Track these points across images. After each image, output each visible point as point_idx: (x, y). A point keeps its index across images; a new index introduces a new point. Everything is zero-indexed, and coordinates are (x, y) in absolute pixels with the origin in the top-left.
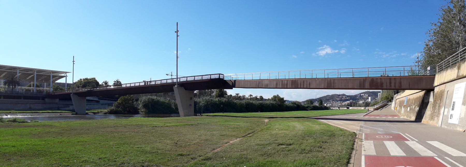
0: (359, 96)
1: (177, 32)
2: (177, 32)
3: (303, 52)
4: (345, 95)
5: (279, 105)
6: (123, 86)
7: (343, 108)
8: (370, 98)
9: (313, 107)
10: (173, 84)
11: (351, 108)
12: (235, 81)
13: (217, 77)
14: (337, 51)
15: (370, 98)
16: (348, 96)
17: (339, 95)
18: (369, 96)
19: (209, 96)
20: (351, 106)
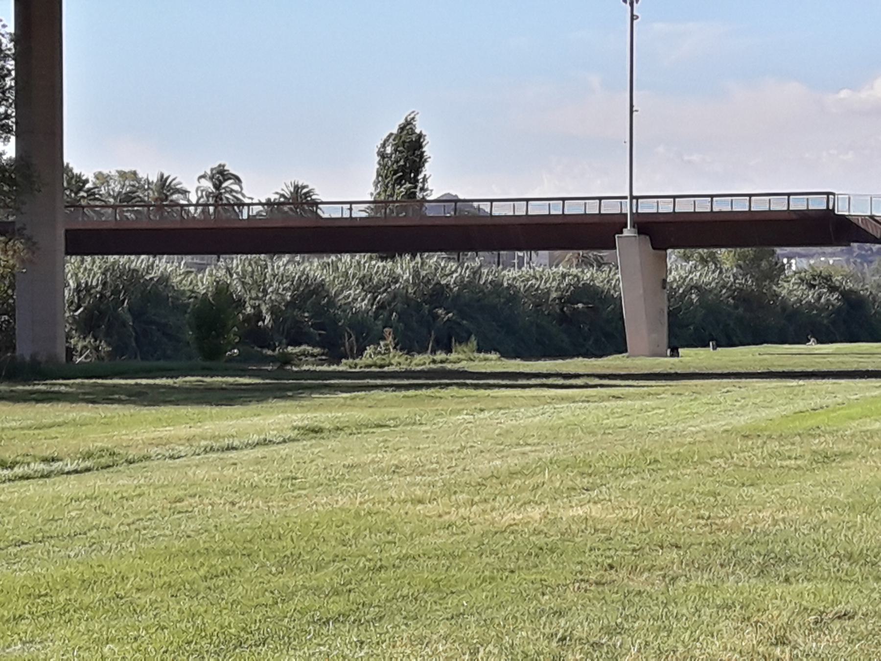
5: (743, 298)
6: (326, 212)
10: (616, 223)
13: (818, 204)
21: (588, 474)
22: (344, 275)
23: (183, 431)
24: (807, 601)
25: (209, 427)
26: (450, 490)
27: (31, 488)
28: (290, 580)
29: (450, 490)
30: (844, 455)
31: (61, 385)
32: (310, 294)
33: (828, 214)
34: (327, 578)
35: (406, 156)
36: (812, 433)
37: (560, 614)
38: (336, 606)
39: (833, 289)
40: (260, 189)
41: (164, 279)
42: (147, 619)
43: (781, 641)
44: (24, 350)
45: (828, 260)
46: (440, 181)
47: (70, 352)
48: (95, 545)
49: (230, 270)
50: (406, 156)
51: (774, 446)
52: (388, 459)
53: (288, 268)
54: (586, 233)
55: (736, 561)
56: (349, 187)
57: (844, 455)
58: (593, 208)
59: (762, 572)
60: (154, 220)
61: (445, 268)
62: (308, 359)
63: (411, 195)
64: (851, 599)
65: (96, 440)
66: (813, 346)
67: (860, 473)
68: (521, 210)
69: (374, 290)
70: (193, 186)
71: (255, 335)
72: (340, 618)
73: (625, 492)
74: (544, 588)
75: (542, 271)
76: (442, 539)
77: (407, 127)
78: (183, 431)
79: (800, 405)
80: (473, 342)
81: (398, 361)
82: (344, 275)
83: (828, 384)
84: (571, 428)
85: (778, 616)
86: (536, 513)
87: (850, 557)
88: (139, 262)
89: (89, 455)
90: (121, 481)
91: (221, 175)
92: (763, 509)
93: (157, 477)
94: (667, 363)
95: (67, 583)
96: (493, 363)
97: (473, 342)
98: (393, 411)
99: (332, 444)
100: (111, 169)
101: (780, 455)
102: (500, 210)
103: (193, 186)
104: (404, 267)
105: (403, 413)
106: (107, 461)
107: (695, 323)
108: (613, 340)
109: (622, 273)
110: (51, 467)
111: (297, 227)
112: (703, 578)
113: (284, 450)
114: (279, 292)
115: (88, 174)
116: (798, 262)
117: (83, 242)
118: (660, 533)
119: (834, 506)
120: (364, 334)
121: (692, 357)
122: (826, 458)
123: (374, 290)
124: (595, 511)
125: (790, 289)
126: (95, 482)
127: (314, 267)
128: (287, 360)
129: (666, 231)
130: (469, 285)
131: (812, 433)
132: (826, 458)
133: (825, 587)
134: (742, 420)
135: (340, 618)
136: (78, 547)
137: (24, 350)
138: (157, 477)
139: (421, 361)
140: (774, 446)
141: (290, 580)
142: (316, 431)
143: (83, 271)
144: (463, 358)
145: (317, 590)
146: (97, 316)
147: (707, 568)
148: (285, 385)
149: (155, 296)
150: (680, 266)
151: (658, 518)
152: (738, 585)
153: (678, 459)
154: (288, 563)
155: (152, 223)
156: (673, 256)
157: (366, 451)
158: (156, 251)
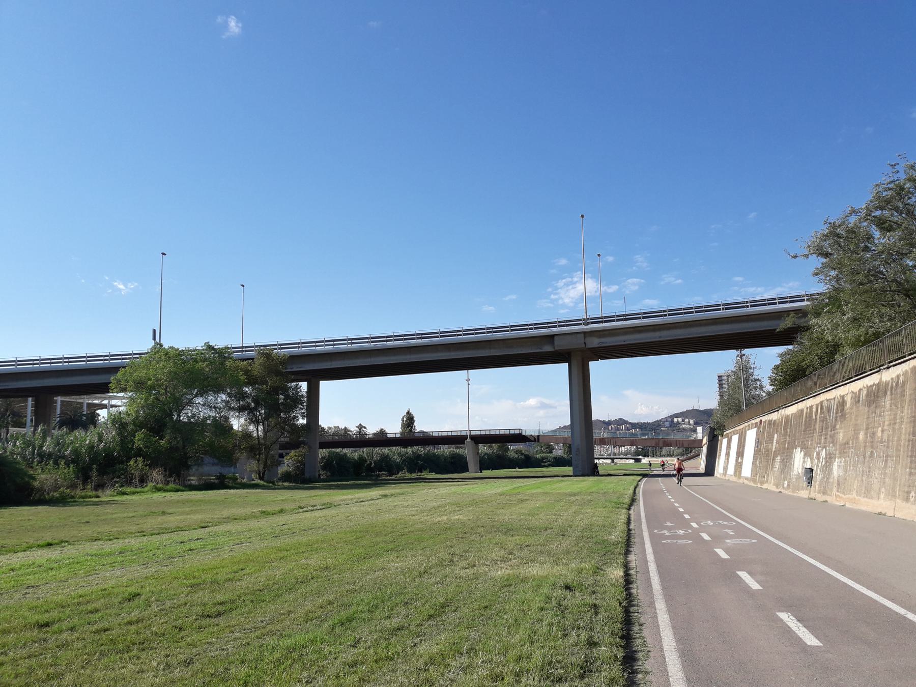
0: (667, 424)
1: (468, 380)
2: (468, 380)
3: (514, 297)
4: (626, 422)
5: (498, 456)
6: (389, 436)
7: (623, 461)
8: (700, 429)
9: (555, 458)
10: (465, 437)
11: (645, 461)
12: (538, 436)
13: (517, 432)
14: (614, 288)
15: (700, 429)
16: (634, 426)
17: (608, 423)
18: (697, 424)
19: (230, 424)
20: (645, 455)
21: (459, 506)
22: (394, 453)
23: (350, 497)
24: (518, 542)
25: (357, 495)
26: (422, 512)
27: (308, 515)
28: (378, 539)
29: (422, 512)
30: (527, 500)
31: (317, 485)
32: (385, 458)
33: (520, 434)
34: (388, 538)
35: (409, 420)
36: (517, 494)
37: (452, 547)
38: (391, 546)
39: (522, 454)
40: (371, 430)
41: (345, 454)
42: (339, 551)
43: (511, 554)
44: (307, 475)
45: (520, 446)
46: (420, 426)
47: (319, 475)
48: (325, 530)
49: (364, 451)
50: (409, 420)
51: (508, 497)
52: (405, 504)
53: (378, 451)
54: (456, 440)
55: (498, 531)
56: (394, 429)
57: (527, 500)
58: (459, 434)
59: (506, 534)
60: (343, 439)
61: (421, 450)
62: (384, 475)
63: (411, 431)
64: (530, 541)
65: (327, 500)
66: (517, 469)
67: (530, 505)
68: (440, 434)
69: (402, 456)
70: (353, 429)
71: (370, 469)
72: (392, 550)
73: (469, 511)
74: (447, 539)
75: (446, 450)
76: (420, 526)
77: (408, 413)
78: (350, 497)
79: (515, 486)
80: (681, 647)
81: (408, 476)
82: (394, 453)
83: (522, 480)
84: (454, 493)
85: (510, 546)
86: (445, 518)
87: (529, 529)
88: (338, 450)
89: (324, 504)
90: (333, 511)
91: (360, 427)
92: (507, 515)
93: (342, 510)
94: (479, 475)
95: (317, 541)
96: (433, 475)
97: (681, 647)
98: (406, 490)
99: (390, 499)
100: (332, 426)
101: (509, 500)
102: (434, 434)
103: (353, 429)
104: (409, 450)
105: (409, 490)
106: (329, 506)
107: (487, 463)
108: (464, 468)
109: (466, 451)
110: (314, 508)
111: (381, 439)
112: (489, 536)
113: (377, 501)
114: (376, 457)
115: (326, 427)
116: (512, 447)
117: (323, 445)
118: (478, 523)
119: (524, 514)
120: (399, 468)
121: (486, 473)
122: (522, 501)
123: (402, 456)
124: (461, 517)
125: (512, 455)
126: (325, 512)
127: (386, 450)
128: (379, 476)
129: (479, 439)
130: (426, 455)
131: (517, 494)
132: (522, 501)
133: (522, 538)
134: (499, 490)
135: (392, 550)
136: (321, 531)
137: (307, 475)
138: (342, 510)
139: (414, 475)
140: (508, 497)
141: (378, 539)
142: (386, 496)
143: (323, 453)
144: (425, 474)
145: (385, 542)
146: (328, 464)
147: (491, 533)
148: (377, 483)
149: (343, 459)
150: (483, 449)
151: (478, 519)
152: (500, 538)
153: (483, 501)
154: (378, 534)
155: (343, 439)
156: (480, 446)
157: (398, 501)
158: (343, 448)
